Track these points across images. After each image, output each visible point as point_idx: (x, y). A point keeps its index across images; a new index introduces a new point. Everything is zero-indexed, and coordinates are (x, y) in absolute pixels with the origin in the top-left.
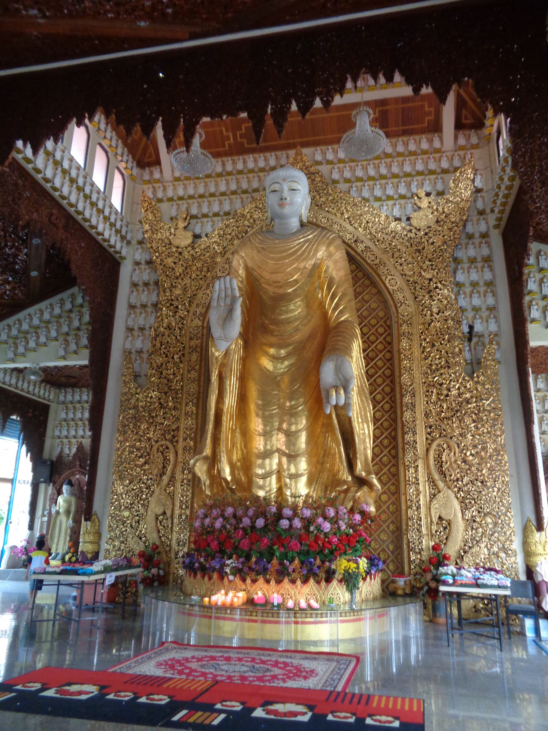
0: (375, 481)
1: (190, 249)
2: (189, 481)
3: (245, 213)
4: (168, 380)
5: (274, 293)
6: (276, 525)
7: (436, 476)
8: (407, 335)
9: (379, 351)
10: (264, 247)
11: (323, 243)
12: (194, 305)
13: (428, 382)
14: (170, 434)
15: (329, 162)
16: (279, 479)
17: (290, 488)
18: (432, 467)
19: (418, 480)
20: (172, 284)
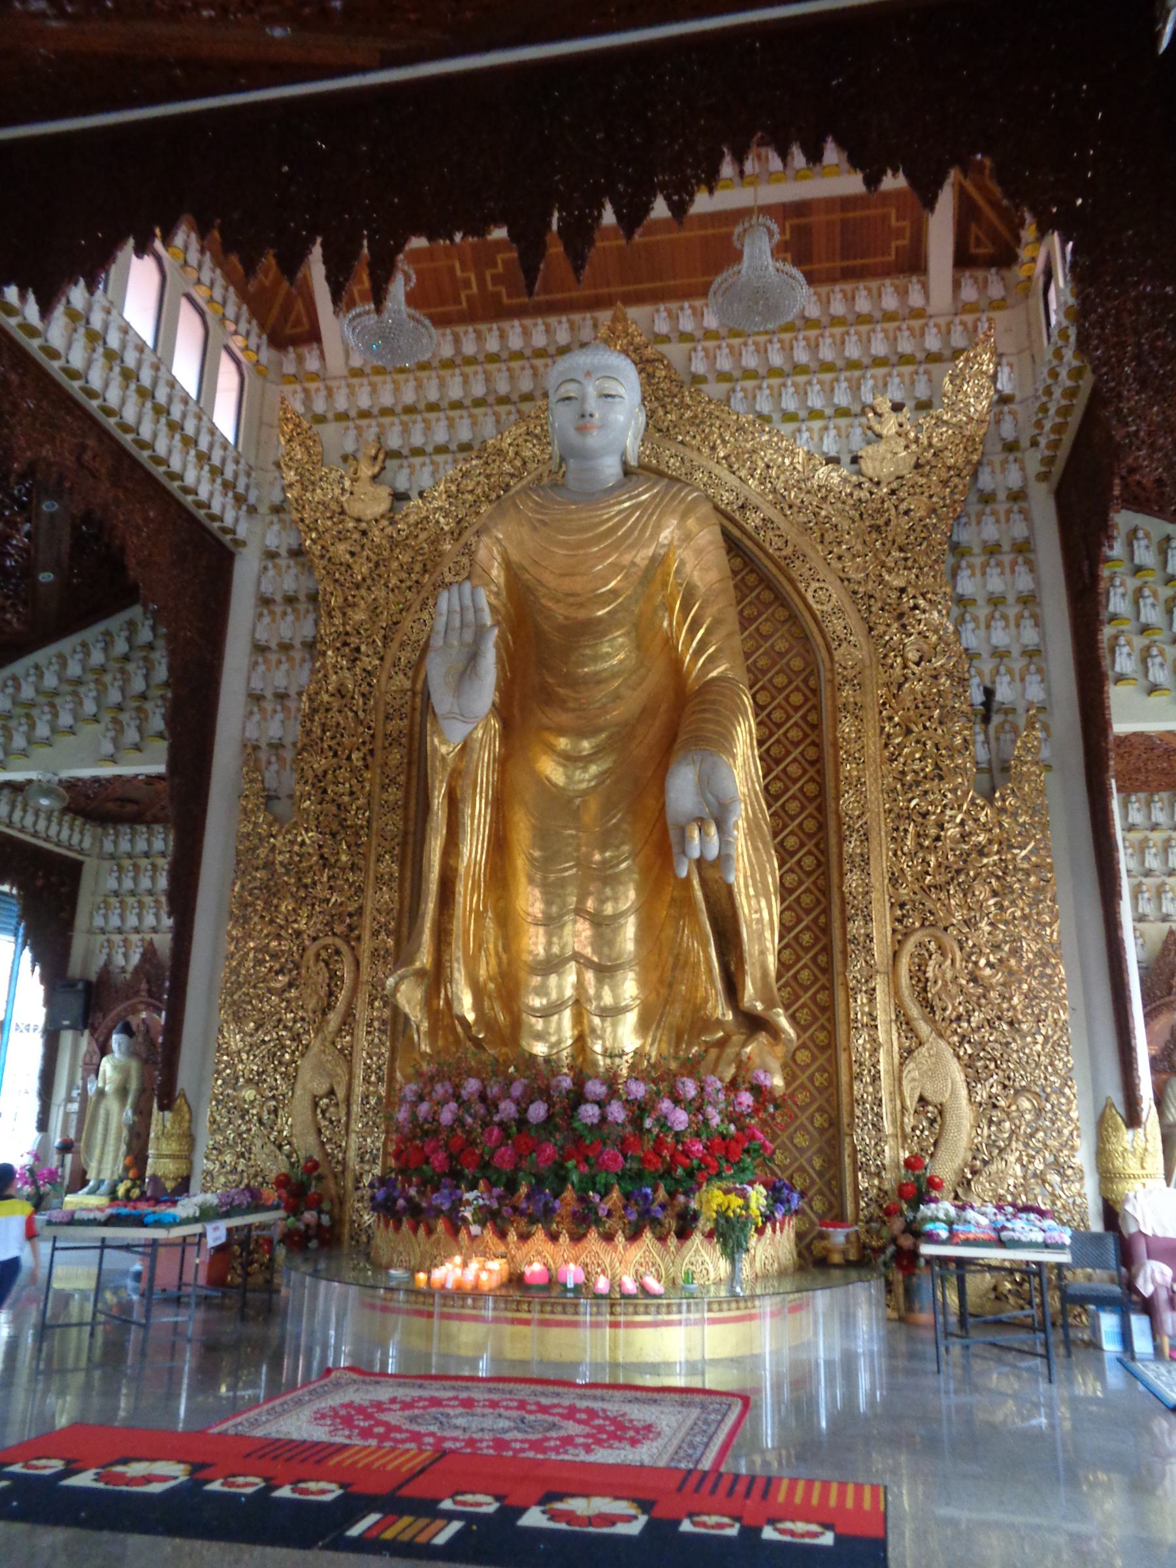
0: (784, 1022)
1: (385, 523)
2: (384, 1022)
3: (505, 445)
4: (339, 806)
5: (566, 618)
6: (572, 1117)
7: (915, 1011)
10: (546, 518)
12: (394, 645)
13: (896, 809)
14: (343, 922)
15: (685, 337)
16: (578, 1019)
17: (602, 1038)
18: (906, 992)
19: (874, 1019)
20: (346, 600)
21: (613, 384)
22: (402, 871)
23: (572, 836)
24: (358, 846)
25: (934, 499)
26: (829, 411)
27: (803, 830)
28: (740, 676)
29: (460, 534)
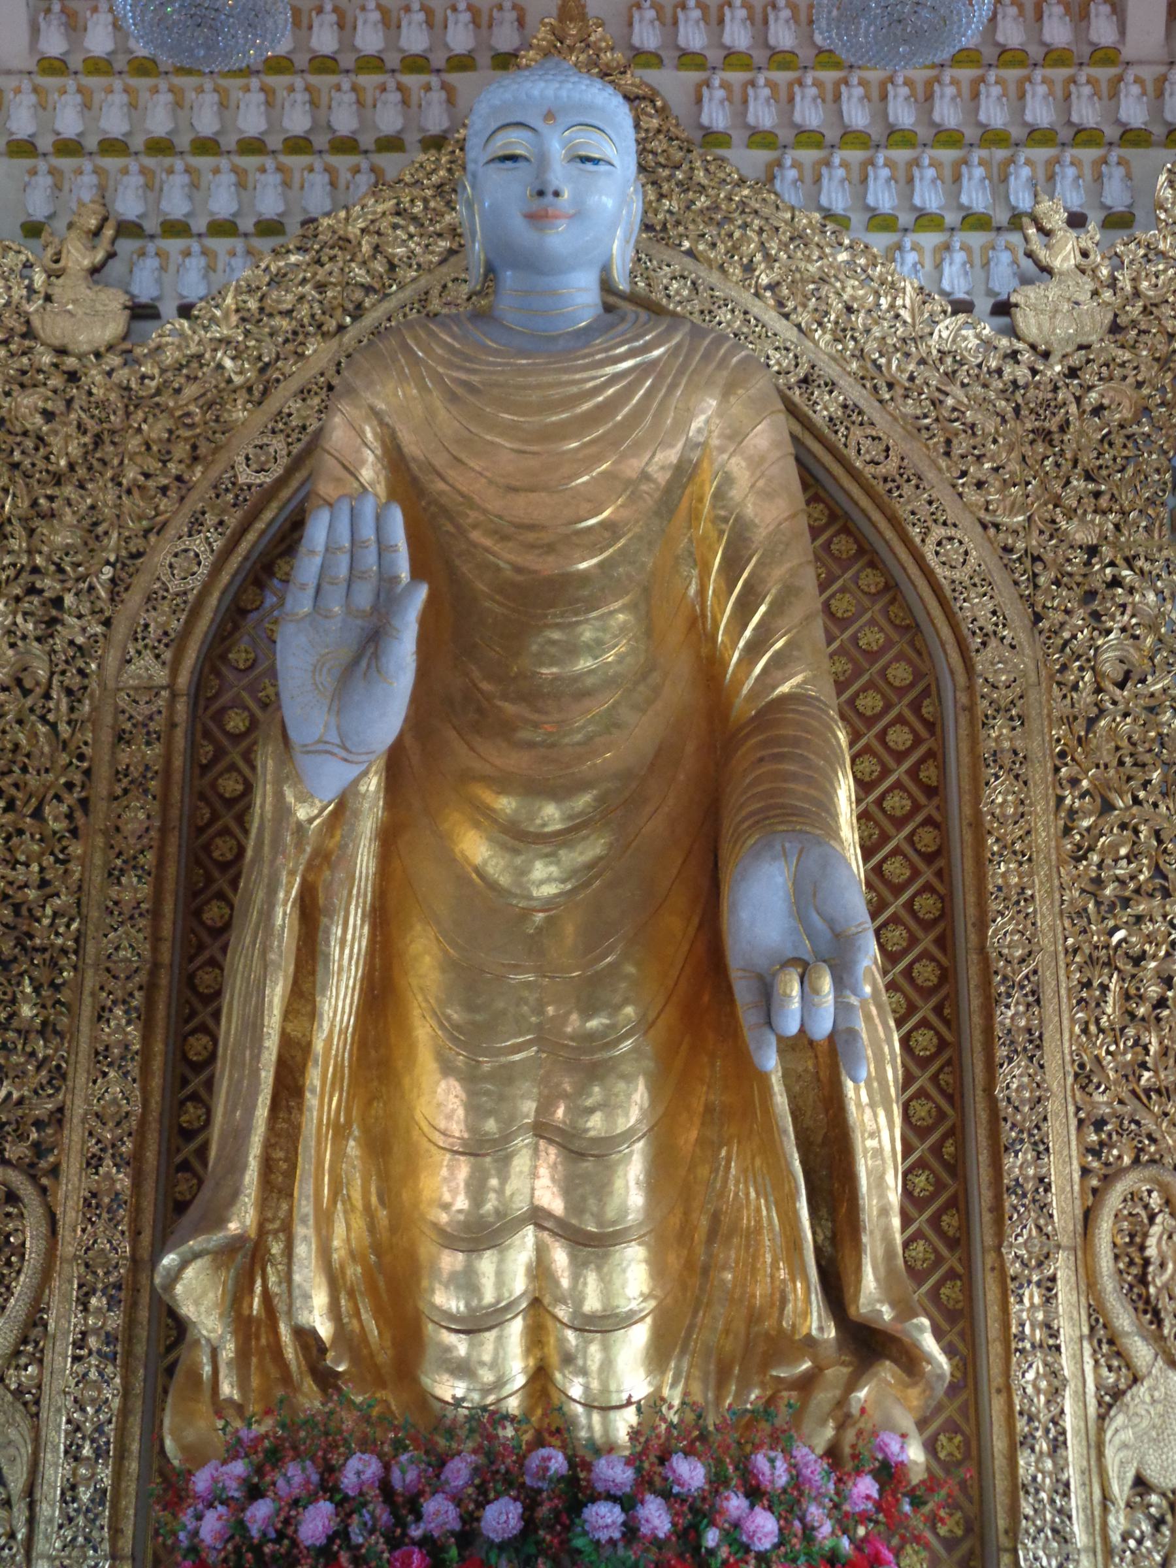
0: (929, 1343)
1: (114, 360)
2: (110, 1339)
3: (353, 230)
4: (17, 908)
5: (519, 570)
6: (567, 1528)
7: (1124, 1319)
8: (1007, 763)
9: (891, 818)
10: (474, 379)
11: (710, 383)
12: (134, 599)
13: (1086, 949)
14: (22, 1137)
15: (688, 59)
16: (536, 1337)
17: (584, 1372)
18: (1108, 1284)
19: (1055, 1335)
20: (34, 504)
21: (596, 136)
22: (146, 1039)
23: (527, 985)
24: (56, 988)
25: (1145, 391)
26: (952, 218)
27: (911, 980)
28: (825, 691)
29: (265, 392)
